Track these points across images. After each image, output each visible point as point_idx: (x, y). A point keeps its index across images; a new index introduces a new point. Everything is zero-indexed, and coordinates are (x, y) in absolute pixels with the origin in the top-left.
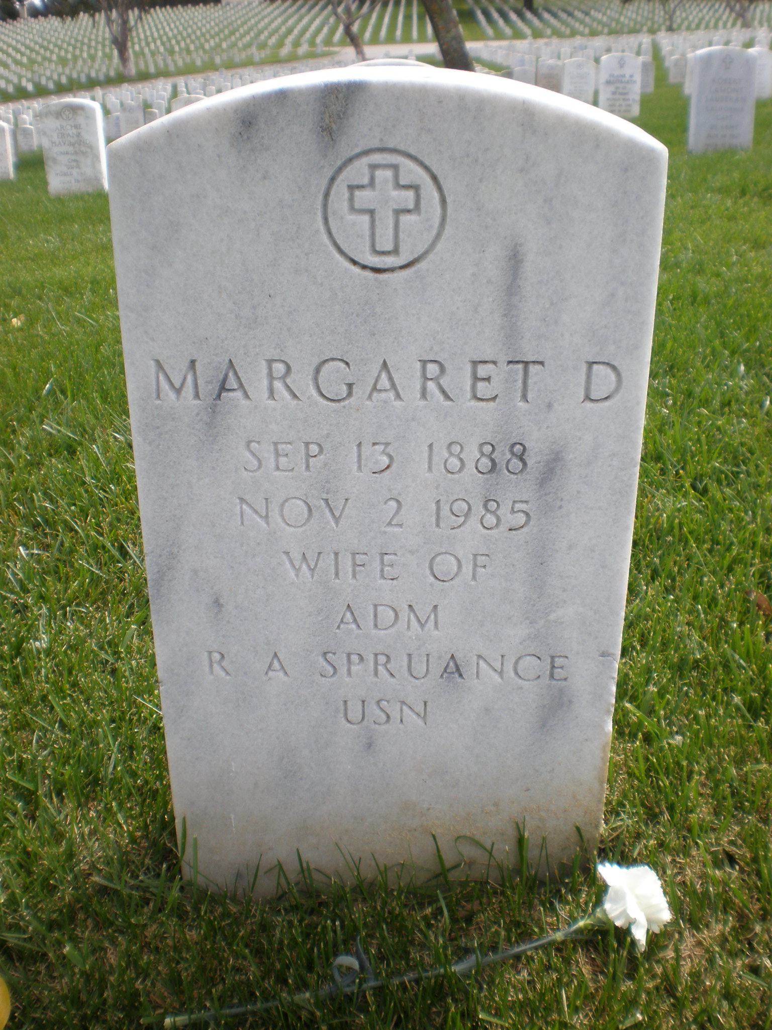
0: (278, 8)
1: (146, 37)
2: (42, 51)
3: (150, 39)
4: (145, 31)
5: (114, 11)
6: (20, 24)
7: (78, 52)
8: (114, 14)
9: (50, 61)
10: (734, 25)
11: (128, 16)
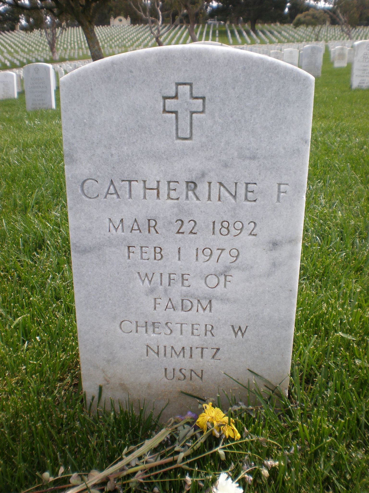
0: (141, 28)
2: (28, 46)
4: (71, 37)
6: (14, 34)
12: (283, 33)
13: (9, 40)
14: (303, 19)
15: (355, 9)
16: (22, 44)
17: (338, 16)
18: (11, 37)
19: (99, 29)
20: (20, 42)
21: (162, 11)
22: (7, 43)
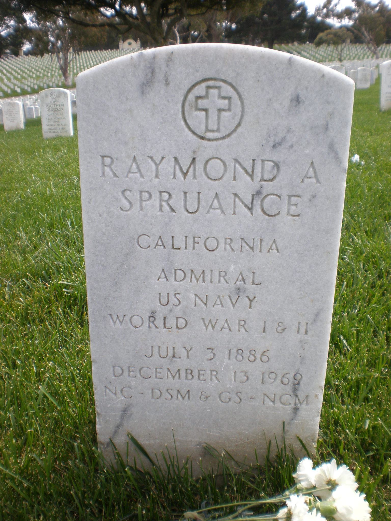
1: (80, 66)
2: (35, 72)
3: (82, 67)
4: (80, 63)
5: (61, 53)
6: (19, 59)
7: (46, 73)
8: (61, 55)
9: (48, 77)
10: (372, 57)
11: (68, 55)
12: (302, 52)
13: (15, 66)
14: (325, 38)
15: (381, 26)
16: (28, 70)
17: (363, 34)
18: (15, 63)
19: (97, 54)
20: (26, 68)
21: (179, 32)
22: (13, 69)
